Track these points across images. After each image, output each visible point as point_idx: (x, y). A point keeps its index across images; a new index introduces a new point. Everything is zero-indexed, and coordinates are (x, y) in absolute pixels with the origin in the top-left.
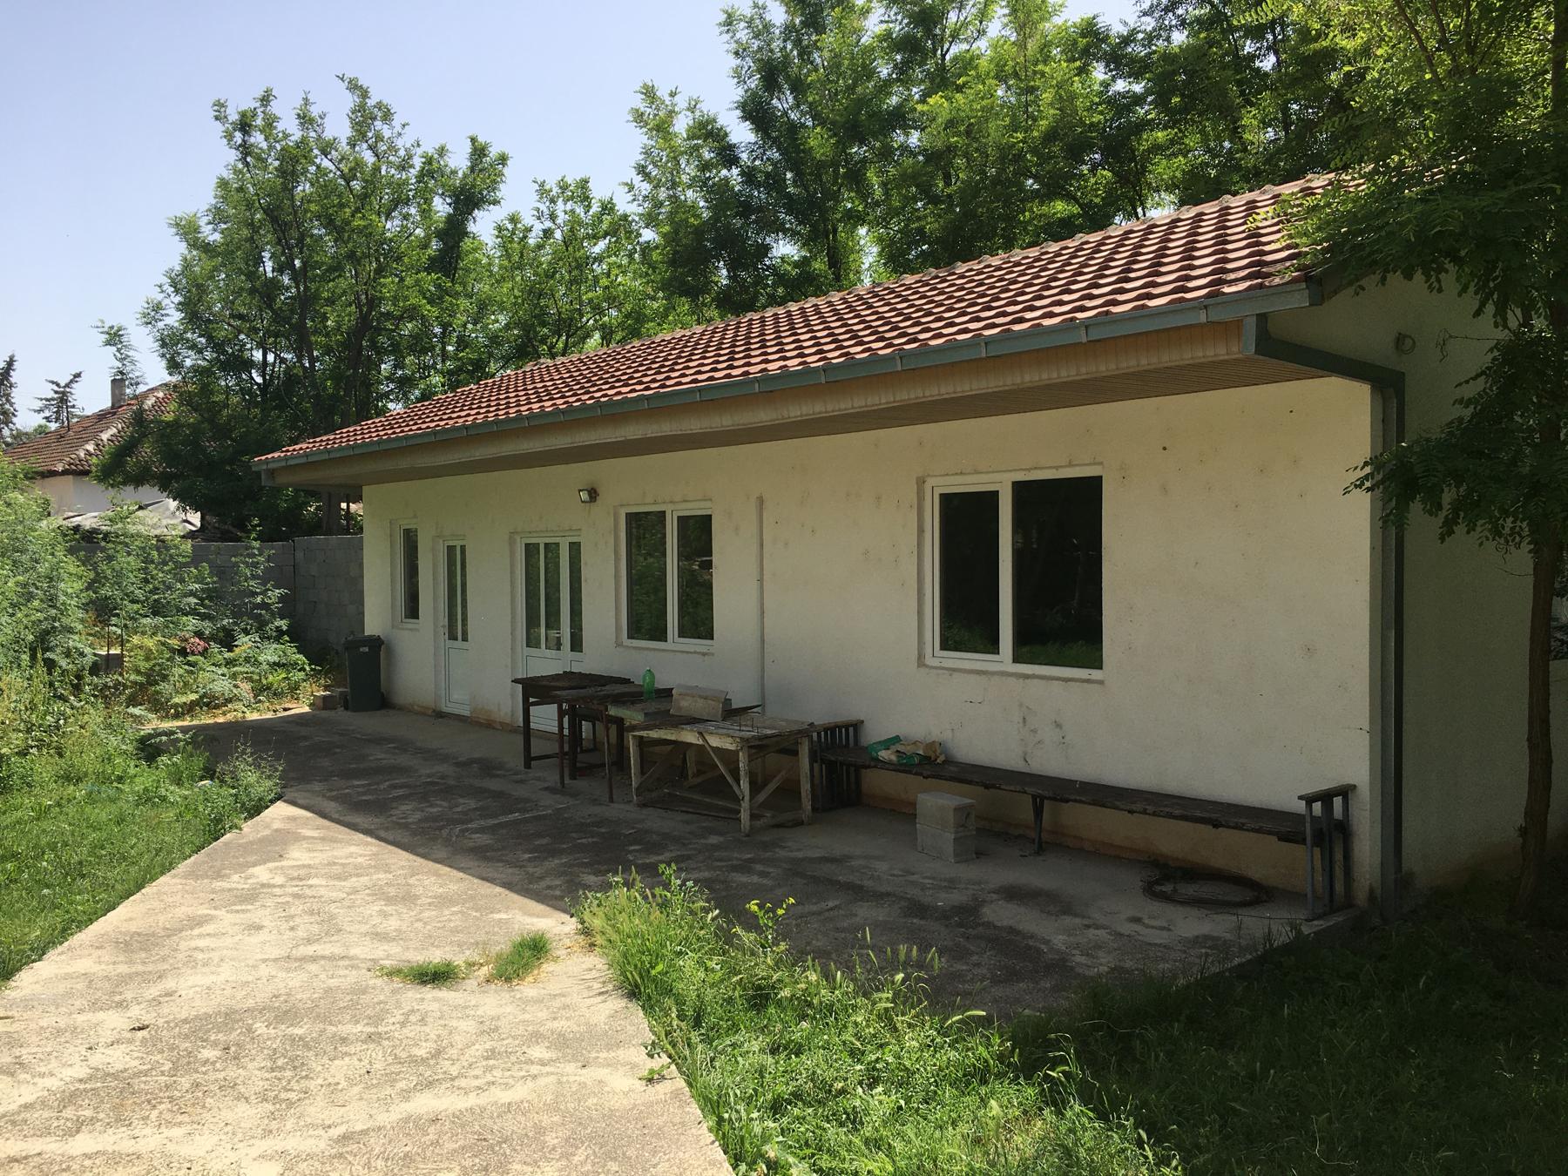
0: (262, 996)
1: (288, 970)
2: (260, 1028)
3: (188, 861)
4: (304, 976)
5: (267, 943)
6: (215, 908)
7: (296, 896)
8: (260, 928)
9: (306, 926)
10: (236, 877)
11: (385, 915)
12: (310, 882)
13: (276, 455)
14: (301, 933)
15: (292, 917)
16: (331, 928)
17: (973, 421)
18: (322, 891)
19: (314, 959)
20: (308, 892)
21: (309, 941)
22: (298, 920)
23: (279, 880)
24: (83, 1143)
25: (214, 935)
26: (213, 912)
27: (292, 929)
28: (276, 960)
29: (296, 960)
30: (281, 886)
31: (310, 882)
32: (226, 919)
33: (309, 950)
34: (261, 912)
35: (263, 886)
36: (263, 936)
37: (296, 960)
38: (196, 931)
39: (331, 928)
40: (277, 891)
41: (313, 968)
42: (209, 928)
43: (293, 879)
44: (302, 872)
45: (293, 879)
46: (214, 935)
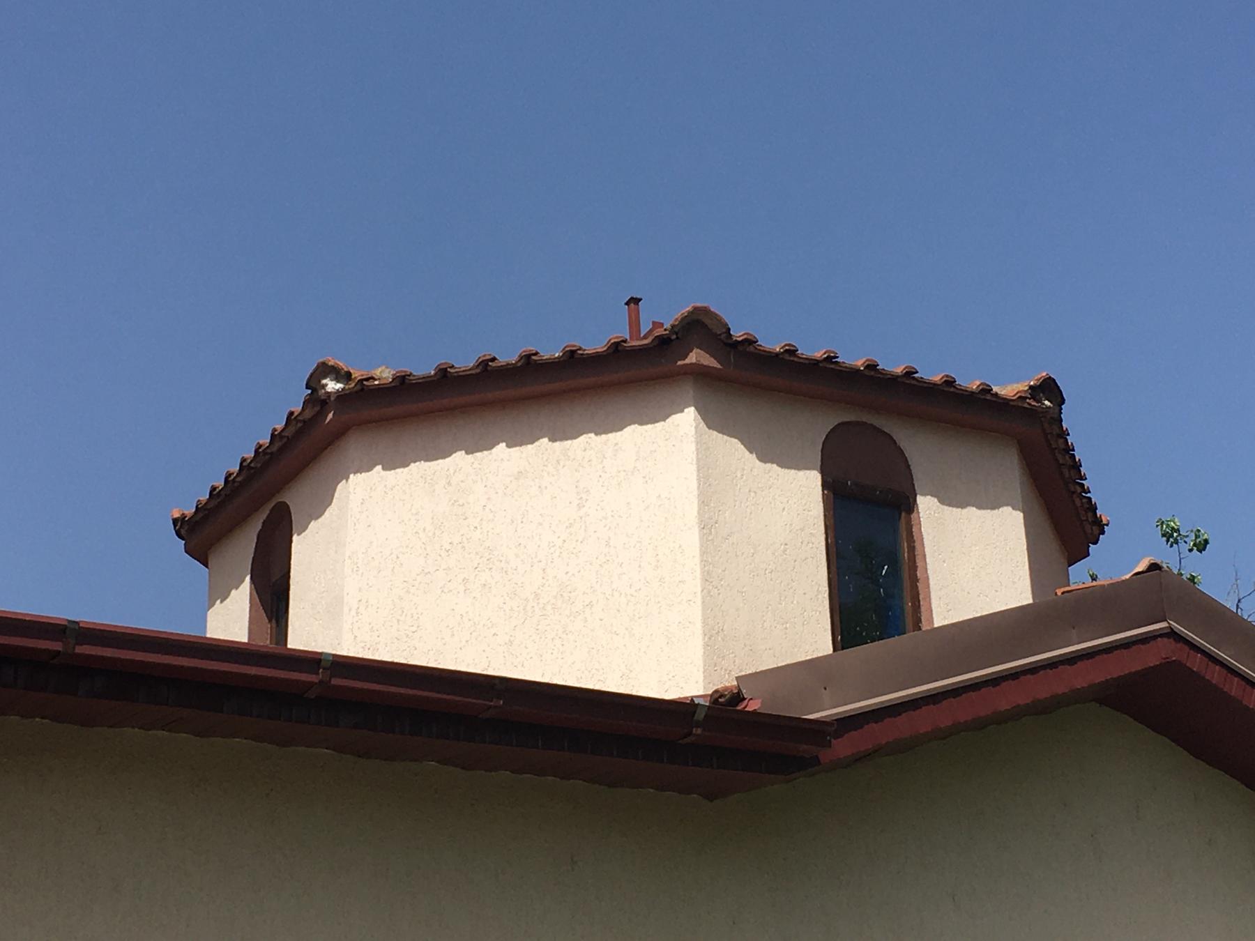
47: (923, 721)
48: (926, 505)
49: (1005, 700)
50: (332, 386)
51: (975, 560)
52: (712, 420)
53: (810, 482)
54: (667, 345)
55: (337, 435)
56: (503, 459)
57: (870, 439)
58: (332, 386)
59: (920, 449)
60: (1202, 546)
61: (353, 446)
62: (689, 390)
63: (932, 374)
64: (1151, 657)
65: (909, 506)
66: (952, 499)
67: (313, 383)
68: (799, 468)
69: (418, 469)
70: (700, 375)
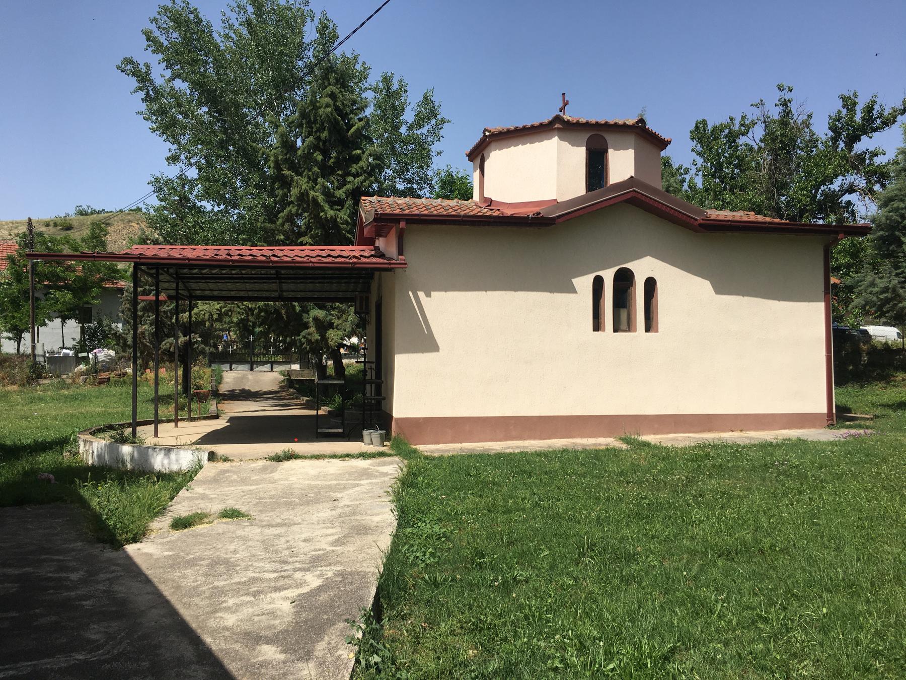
0: (298, 511)
1: (289, 519)
2: (297, 500)
3: (373, 591)
4: (282, 517)
5: (298, 534)
6: (333, 551)
7: (285, 562)
8: (305, 541)
9: (281, 544)
10: (330, 574)
11: (235, 552)
12: (276, 575)
13: (283, 312)
14: (283, 540)
15: (288, 548)
16: (267, 545)
17: (776, 303)
18: (268, 566)
19: (278, 525)
20: (278, 566)
21: (279, 536)
22: (285, 546)
23: (298, 575)
24: (335, 482)
25: (327, 535)
26: (332, 548)
27: (288, 541)
28: (295, 524)
29: (285, 525)
30: (295, 570)
31: (276, 575)
32: (324, 545)
33: (277, 531)
34: (306, 550)
35: (308, 570)
36: (303, 536)
37: (285, 525)
38: (336, 537)
39: (267, 545)
40: (298, 565)
41: (279, 521)
42: (331, 539)
43: (288, 577)
44: (281, 583)
45: (288, 577)
46: (327, 535)
47: (577, 214)
48: (610, 151)
49: (603, 205)
50: (487, 134)
51: (622, 165)
52: (561, 139)
53: (583, 150)
54: (551, 123)
55: (489, 143)
56: (520, 147)
57: (596, 140)
58: (487, 134)
59: (610, 138)
60: (791, 91)
61: (493, 145)
62: (556, 132)
63: (611, 122)
64: (629, 196)
65: (607, 152)
66: (617, 148)
67: (484, 132)
68: (516, 290)
69: (505, 150)
70: (558, 129)
